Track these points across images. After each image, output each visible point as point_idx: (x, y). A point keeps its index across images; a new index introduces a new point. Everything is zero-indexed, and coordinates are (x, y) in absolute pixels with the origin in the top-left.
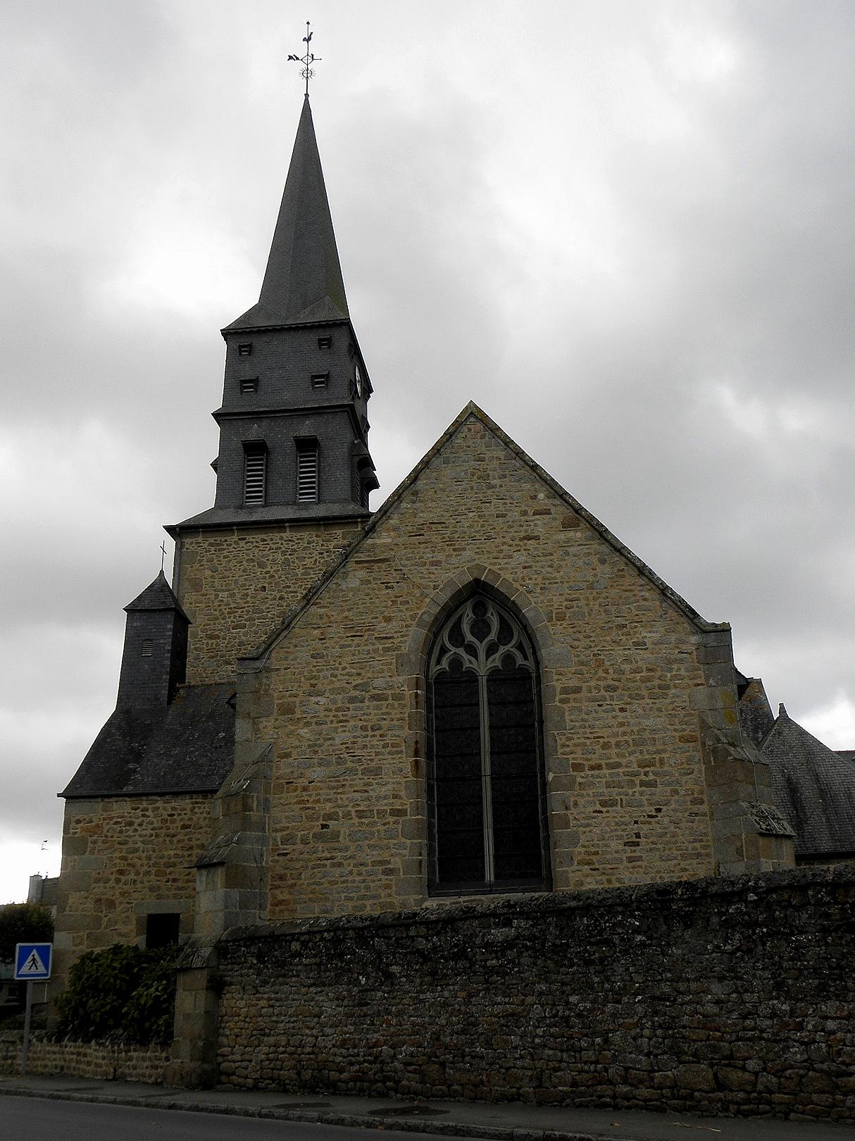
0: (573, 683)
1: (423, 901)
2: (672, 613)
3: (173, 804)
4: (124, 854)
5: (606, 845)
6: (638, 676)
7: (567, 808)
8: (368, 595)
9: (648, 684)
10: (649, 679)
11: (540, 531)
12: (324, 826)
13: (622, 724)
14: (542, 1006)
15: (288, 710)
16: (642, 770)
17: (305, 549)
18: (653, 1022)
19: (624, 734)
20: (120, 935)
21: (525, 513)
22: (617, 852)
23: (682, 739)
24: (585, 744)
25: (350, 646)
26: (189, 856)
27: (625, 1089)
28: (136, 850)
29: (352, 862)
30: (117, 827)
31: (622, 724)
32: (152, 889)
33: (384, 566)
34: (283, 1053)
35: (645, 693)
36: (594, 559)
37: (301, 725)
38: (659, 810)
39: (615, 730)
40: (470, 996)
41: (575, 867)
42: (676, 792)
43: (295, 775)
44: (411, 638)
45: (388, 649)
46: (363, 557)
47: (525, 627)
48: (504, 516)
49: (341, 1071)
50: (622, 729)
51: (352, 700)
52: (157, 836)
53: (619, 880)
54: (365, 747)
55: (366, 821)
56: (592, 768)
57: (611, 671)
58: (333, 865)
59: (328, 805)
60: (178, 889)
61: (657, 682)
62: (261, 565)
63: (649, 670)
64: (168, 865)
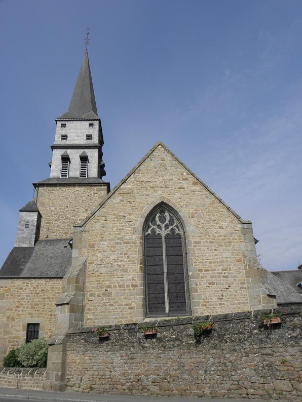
0: (198, 240)
1: (144, 319)
2: (231, 216)
3: (38, 282)
4: (19, 300)
5: (211, 299)
6: (221, 238)
7: (197, 285)
8: (123, 205)
9: (225, 241)
10: (224, 240)
11: (185, 186)
12: (106, 290)
13: (216, 255)
14: (214, 358)
15: (92, 246)
16: (223, 272)
17: (83, 193)
18: (263, 364)
19: (216, 258)
20: (16, 331)
21: (179, 179)
22: (215, 301)
23: (237, 261)
24: (203, 262)
25: (116, 223)
26: (44, 301)
27: (252, 391)
28: (24, 299)
29: (117, 304)
30: (17, 290)
31: (216, 255)
32: (29, 314)
33: (129, 195)
34: (96, 378)
35: (223, 244)
36: (204, 197)
37: (97, 252)
38: (230, 286)
39: (213, 257)
40: (181, 355)
41: (200, 307)
42: (235, 280)
43: (95, 270)
44: (139, 222)
45: (130, 225)
46: (121, 192)
47: (179, 219)
48: (172, 180)
49: (123, 385)
50: (215, 257)
51: (117, 243)
52: (32, 294)
53: (217, 312)
54: (122, 261)
55: (122, 289)
56: (205, 271)
57: (211, 236)
58: (110, 305)
59: (108, 282)
60: (39, 314)
61: (227, 240)
62: (67, 198)
63: (225, 236)
64: (36, 305)
